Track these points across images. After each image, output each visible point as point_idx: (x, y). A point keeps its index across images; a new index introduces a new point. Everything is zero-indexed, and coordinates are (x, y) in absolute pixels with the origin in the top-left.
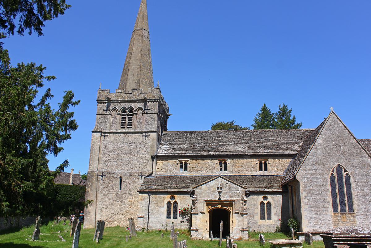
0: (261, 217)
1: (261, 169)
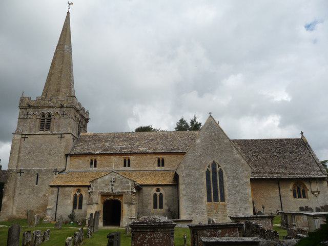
0: (154, 206)
1: (159, 166)
